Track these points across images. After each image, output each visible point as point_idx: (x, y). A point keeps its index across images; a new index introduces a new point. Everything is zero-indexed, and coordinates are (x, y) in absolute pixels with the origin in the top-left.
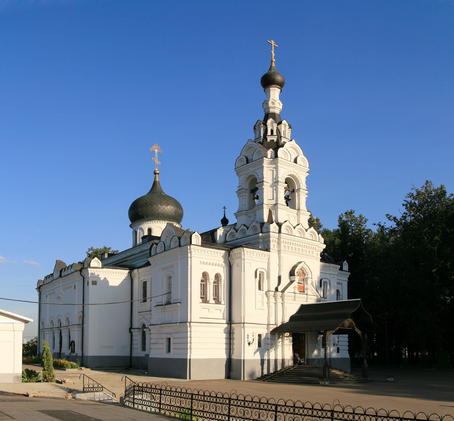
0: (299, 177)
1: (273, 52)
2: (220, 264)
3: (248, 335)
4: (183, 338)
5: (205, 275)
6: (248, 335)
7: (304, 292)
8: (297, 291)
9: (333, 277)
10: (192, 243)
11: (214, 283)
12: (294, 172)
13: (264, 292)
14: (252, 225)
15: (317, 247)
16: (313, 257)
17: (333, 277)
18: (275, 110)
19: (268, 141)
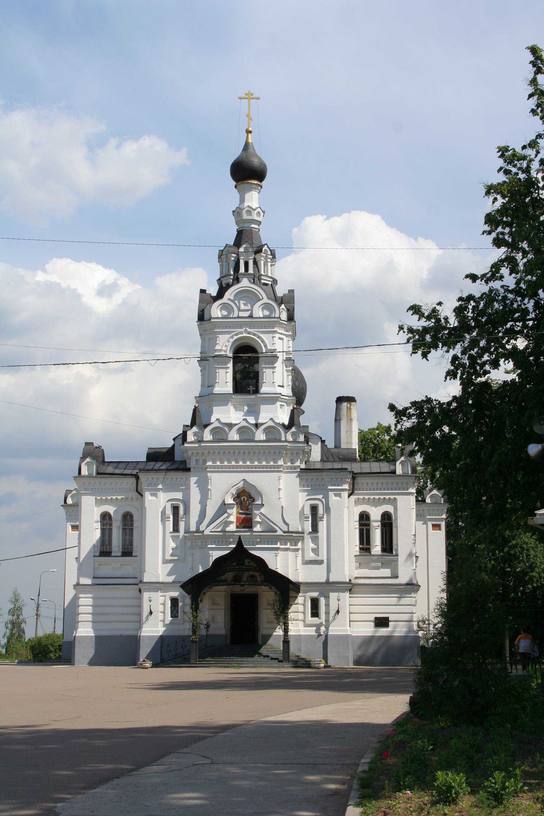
0: (259, 337)
5: (364, 518)
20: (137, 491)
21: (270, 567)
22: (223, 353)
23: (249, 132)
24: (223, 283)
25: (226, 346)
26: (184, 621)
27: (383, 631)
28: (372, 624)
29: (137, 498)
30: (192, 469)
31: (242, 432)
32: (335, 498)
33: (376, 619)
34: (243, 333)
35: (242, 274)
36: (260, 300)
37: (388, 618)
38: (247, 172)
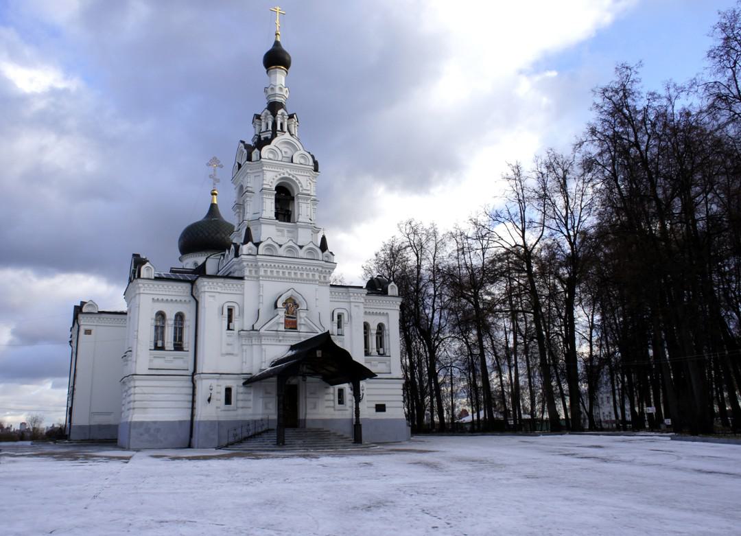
0: (297, 179)
1: (278, 22)
2: (187, 300)
3: (341, 402)
4: (175, 401)
5: (161, 315)
6: (341, 402)
7: (296, 329)
8: (282, 328)
9: (356, 306)
10: (142, 277)
11: (377, 333)
12: (290, 175)
13: (236, 332)
14: (287, 245)
15: (320, 269)
16: (316, 281)
17: (356, 306)
18: (277, 98)
19: (262, 139)
20: (192, 295)
21: (354, 359)
22: (268, 187)
23: (276, 34)
24: (262, 137)
25: (272, 182)
26: (237, 408)
27: (381, 415)
28: (374, 410)
29: (190, 301)
30: (246, 278)
31: (268, 248)
32: (211, 299)
33: (377, 405)
34: (286, 173)
35: (279, 131)
36: (297, 150)
37: (384, 405)
38: (276, 59)
